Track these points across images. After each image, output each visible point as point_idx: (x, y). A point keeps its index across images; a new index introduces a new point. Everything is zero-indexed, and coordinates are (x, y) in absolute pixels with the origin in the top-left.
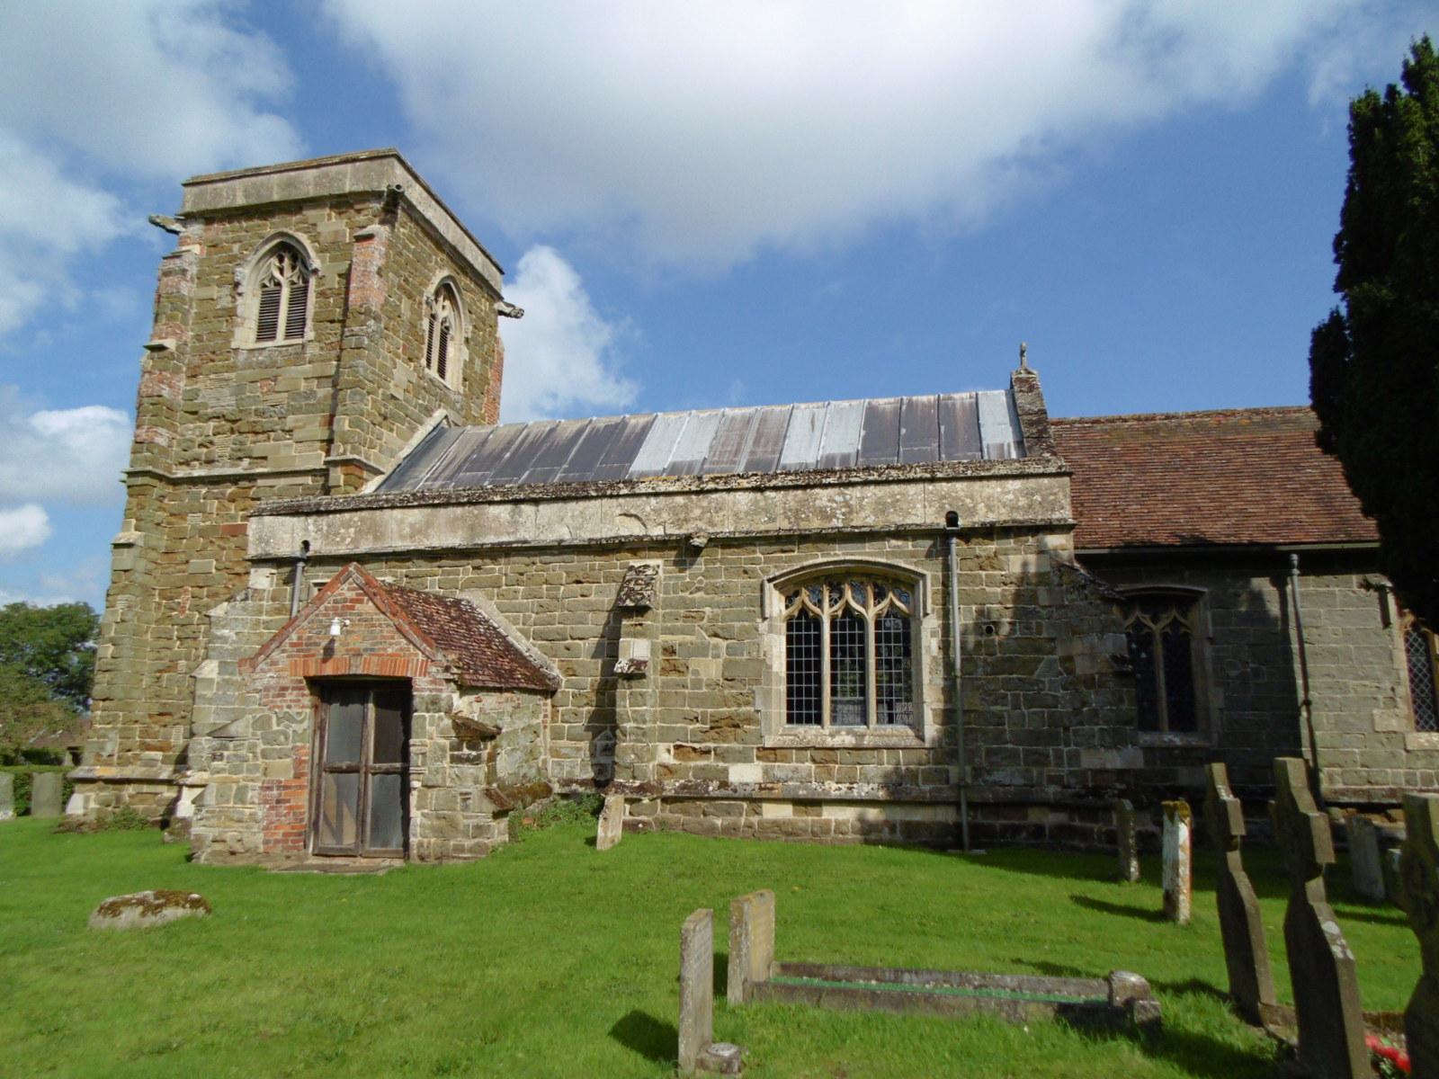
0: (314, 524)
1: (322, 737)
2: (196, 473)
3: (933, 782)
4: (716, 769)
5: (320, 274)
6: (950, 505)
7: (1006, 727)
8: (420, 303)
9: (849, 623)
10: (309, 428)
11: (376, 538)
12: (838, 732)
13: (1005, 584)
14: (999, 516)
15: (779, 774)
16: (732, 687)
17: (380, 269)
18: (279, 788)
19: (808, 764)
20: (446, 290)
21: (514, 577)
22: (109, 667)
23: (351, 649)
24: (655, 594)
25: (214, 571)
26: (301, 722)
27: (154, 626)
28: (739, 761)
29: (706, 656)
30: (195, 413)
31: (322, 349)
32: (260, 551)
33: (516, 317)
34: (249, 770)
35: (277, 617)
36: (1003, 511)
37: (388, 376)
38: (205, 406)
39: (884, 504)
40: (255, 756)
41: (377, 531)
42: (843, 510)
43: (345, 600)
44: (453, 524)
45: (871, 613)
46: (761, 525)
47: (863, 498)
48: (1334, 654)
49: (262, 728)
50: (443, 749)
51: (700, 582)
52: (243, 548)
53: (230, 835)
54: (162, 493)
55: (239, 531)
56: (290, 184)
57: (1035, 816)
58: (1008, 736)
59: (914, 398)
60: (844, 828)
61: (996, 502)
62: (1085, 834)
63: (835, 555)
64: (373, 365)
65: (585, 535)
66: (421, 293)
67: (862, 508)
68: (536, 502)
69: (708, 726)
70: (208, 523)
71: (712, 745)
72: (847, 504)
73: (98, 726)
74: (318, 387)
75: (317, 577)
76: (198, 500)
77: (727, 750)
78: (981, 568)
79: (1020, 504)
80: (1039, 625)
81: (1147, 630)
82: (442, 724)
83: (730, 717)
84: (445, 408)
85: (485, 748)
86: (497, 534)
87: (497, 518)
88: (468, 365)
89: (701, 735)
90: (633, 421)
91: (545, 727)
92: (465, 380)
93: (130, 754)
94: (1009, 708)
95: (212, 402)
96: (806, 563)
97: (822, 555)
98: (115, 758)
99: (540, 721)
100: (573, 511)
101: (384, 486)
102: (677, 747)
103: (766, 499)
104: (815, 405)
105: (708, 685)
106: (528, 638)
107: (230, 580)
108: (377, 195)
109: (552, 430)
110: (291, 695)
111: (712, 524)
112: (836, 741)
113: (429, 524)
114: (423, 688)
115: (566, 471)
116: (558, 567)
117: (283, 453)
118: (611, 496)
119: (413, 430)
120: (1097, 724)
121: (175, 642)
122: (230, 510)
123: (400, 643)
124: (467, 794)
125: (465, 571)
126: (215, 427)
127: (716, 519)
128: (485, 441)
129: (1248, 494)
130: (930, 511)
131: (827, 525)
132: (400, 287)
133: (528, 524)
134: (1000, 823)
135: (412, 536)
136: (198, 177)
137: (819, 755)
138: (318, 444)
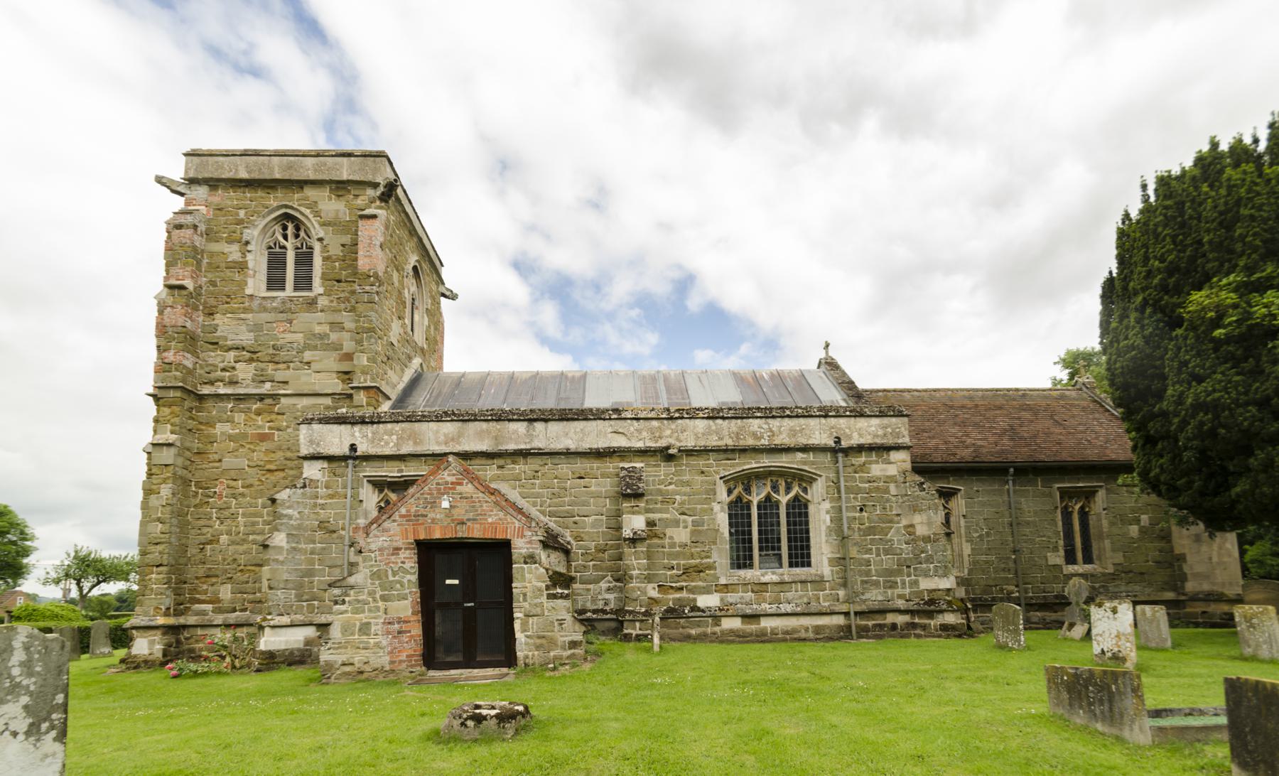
0: (360, 432)
2: (222, 391)
3: (828, 601)
5: (325, 243)
7: (872, 567)
11: (415, 443)
12: (766, 573)
13: (870, 482)
14: (867, 440)
15: (731, 600)
16: (696, 547)
19: (750, 593)
21: (530, 473)
22: (159, 541)
23: (456, 519)
25: (246, 468)
27: (192, 509)
28: (704, 593)
29: (679, 527)
32: (311, 451)
33: (453, 299)
34: (370, 611)
35: (330, 501)
36: (869, 437)
37: (389, 328)
38: (226, 339)
39: (795, 431)
40: (375, 600)
43: (447, 483)
44: (480, 435)
46: (713, 442)
48: (1028, 523)
49: (379, 578)
50: (540, 590)
51: (672, 479)
53: (357, 659)
54: (191, 405)
56: (290, 167)
57: (891, 618)
58: (874, 572)
60: (776, 631)
62: (924, 627)
64: (381, 317)
65: (586, 445)
67: (780, 433)
68: (546, 421)
70: (238, 431)
71: (684, 584)
73: (154, 586)
74: (331, 331)
75: (365, 471)
77: (695, 587)
78: (855, 472)
79: (879, 433)
80: (891, 507)
82: (538, 573)
87: (515, 432)
89: (676, 578)
92: (427, 339)
93: (182, 607)
94: (874, 556)
96: (745, 467)
97: (755, 463)
98: (172, 610)
102: (659, 586)
107: (264, 475)
110: (404, 554)
111: (678, 439)
112: (766, 579)
114: (520, 547)
116: (565, 468)
117: (304, 379)
118: (601, 419)
121: (215, 521)
123: (498, 515)
124: (562, 620)
126: (235, 356)
127: (682, 438)
129: (973, 435)
131: (759, 444)
133: (541, 436)
134: (870, 623)
136: (197, 150)
137: (756, 588)
138: (335, 375)
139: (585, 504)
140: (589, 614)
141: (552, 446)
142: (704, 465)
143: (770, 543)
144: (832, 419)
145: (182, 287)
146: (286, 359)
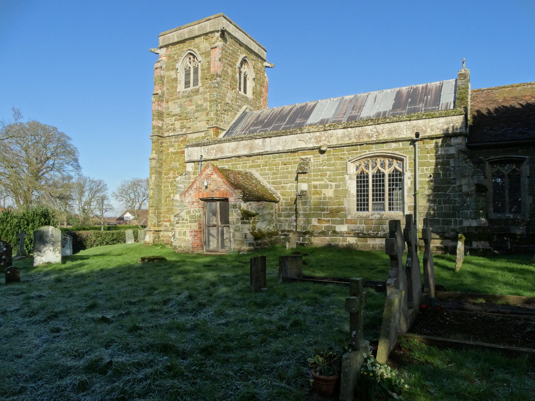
1: (205, 217)
2: (171, 134)
4: (332, 227)
6: (417, 130)
8: (235, 68)
9: (379, 177)
10: (202, 117)
11: (222, 153)
17: (220, 59)
18: (194, 232)
19: (363, 225)
20: (244, 61)
24: (310, 168)
26: (199, 212)
28: (339, 224)
29: (328, 188)
30: (169, 114)
31: (204, 89)
32: (189, 159)
36: (437, 131)
38: (171, 112)
39: (391, 131)
41: (221, 150)
42: (376, 134)
43: (208, 174)
44: (245, 146)
45: (387, 171)
46: (346, 141)
47: (384, 129)
51: (325, 163)
52: (184, 159)
55: (183, 152)
59: (359, 95)
61: (434, 127)
63: (373, 151)
66: (235, 65)
67: (383, 133)
68: (270, 137)
69: (329, 212)
72: (378, 132)
76: (172, 143)
78: (428, 153)
81: (502, 174)
83: (336, 209)
84: (247, 105)
85: (251, 219)
86: (258, 149)
88: (254, 88)
90: (310, 104)
91: (276, 213)
92: (254, 93)
95: (173, 110)
96: (362, 154)
97: (369, 151)
99: (274, 211)
100: (282, 140)
101: (226, 136)
103: (348, 132)
104: (378, 92)
105: (328, 199)
106: (270, 184)
108: (218, 31)
109: (282, 110)
111: (329, 142)
113: (237, 148)
115: (285, 125)
117: (195, 126)
119: (235, 114)
120: (469, 210)
122: (181, 146)
125: (249, 162)
126: (175, 119)
127: (330, 140)
128: (260, 115)
130: (409, 132)
131: (370, 140)
132: (228, 64)
133: (268, 145)
135: (232, 152)
139: (287, 177)
140: (286, 232)
141: (273, 150)
142: (341, 155)
143: (379, 196)
144: (414, 121)
145: (157, 94)
146: (189, 117)
